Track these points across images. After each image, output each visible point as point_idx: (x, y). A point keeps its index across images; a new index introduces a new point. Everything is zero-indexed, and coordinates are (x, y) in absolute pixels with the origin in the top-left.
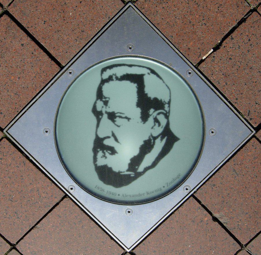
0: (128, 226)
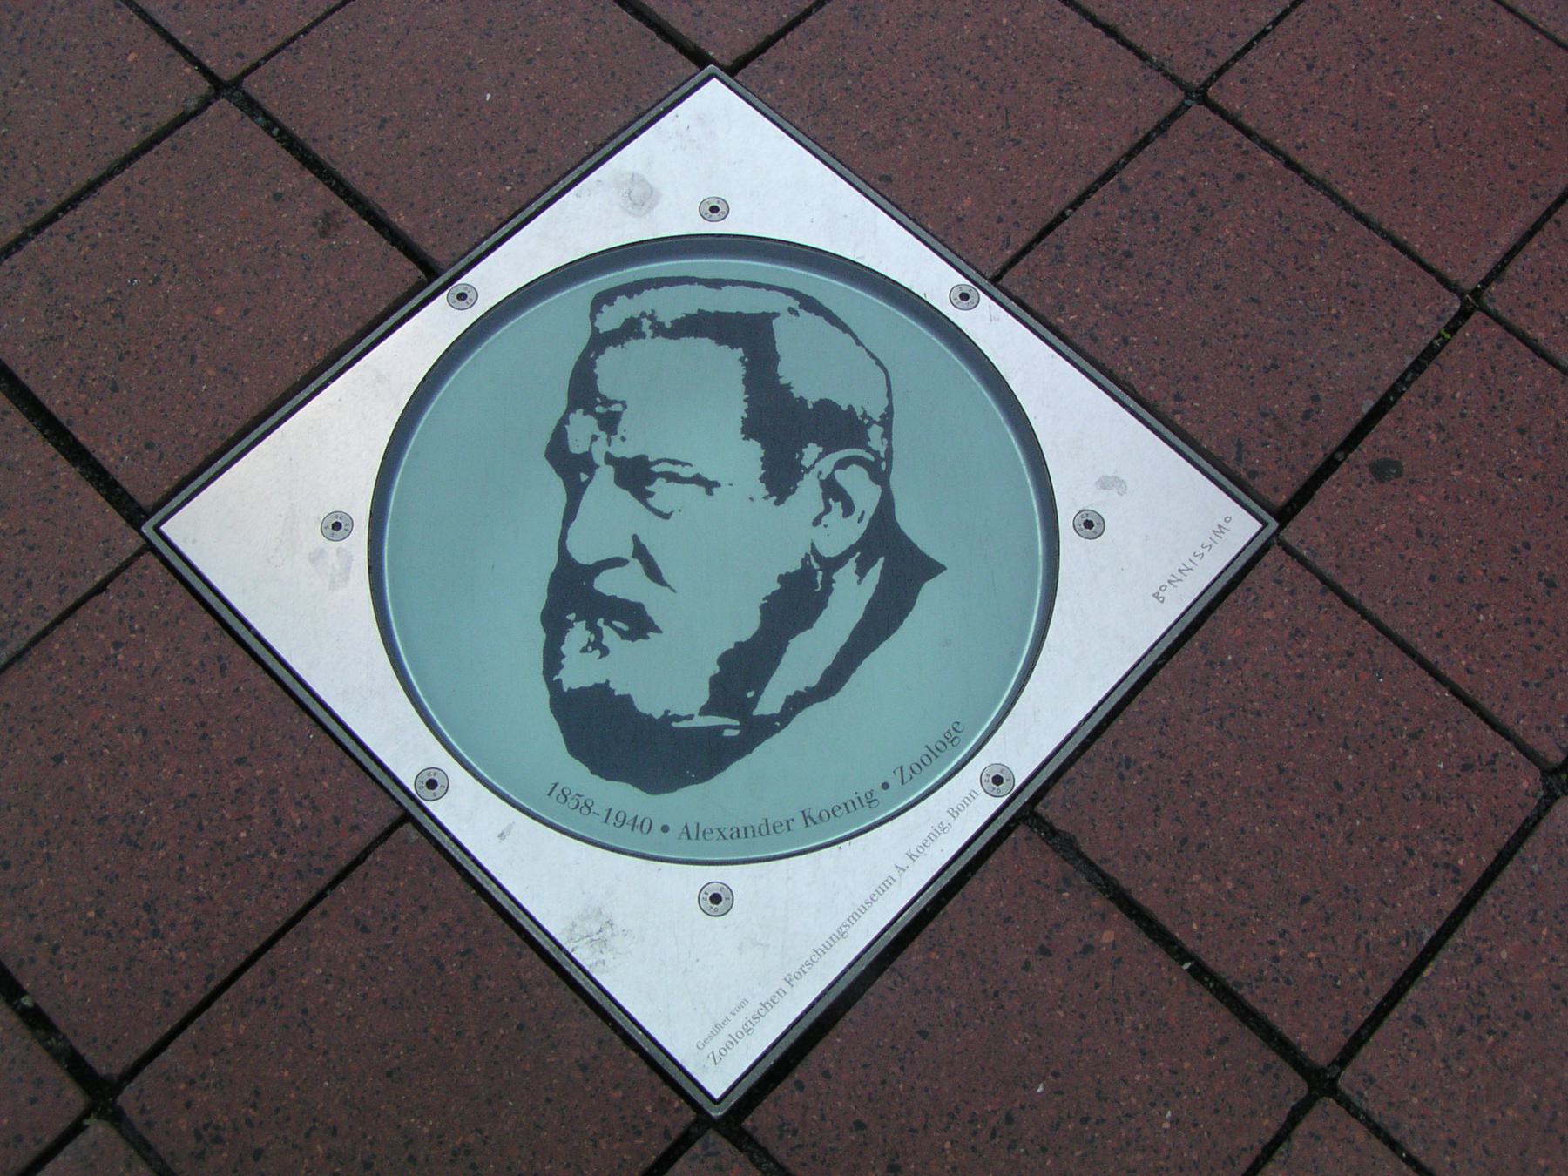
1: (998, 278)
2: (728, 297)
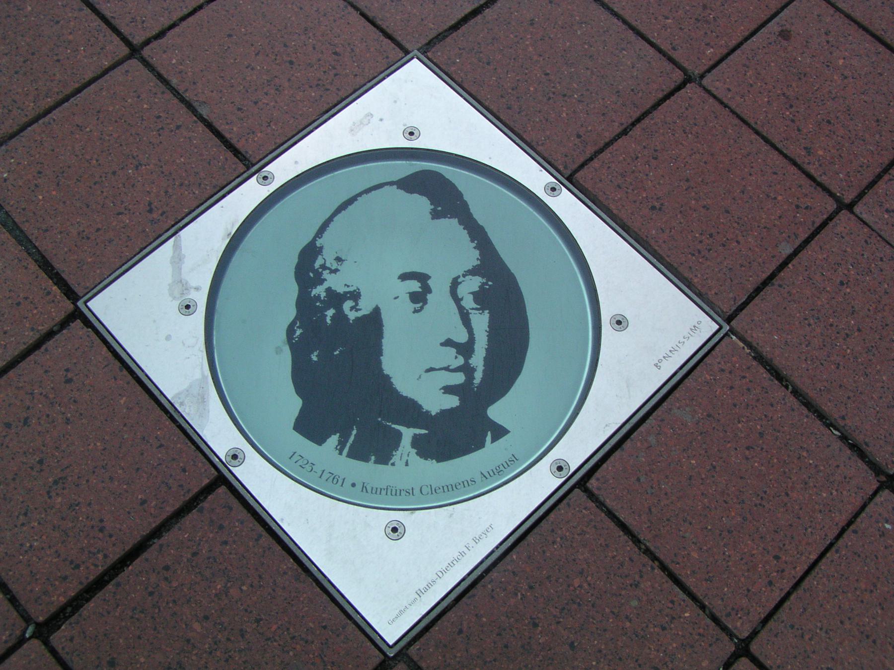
1: (571, 178)
2: (434, 181)
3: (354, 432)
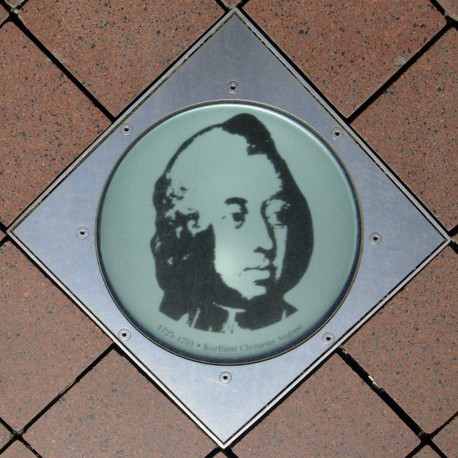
0: (221, 401)
3: (198, 312)
